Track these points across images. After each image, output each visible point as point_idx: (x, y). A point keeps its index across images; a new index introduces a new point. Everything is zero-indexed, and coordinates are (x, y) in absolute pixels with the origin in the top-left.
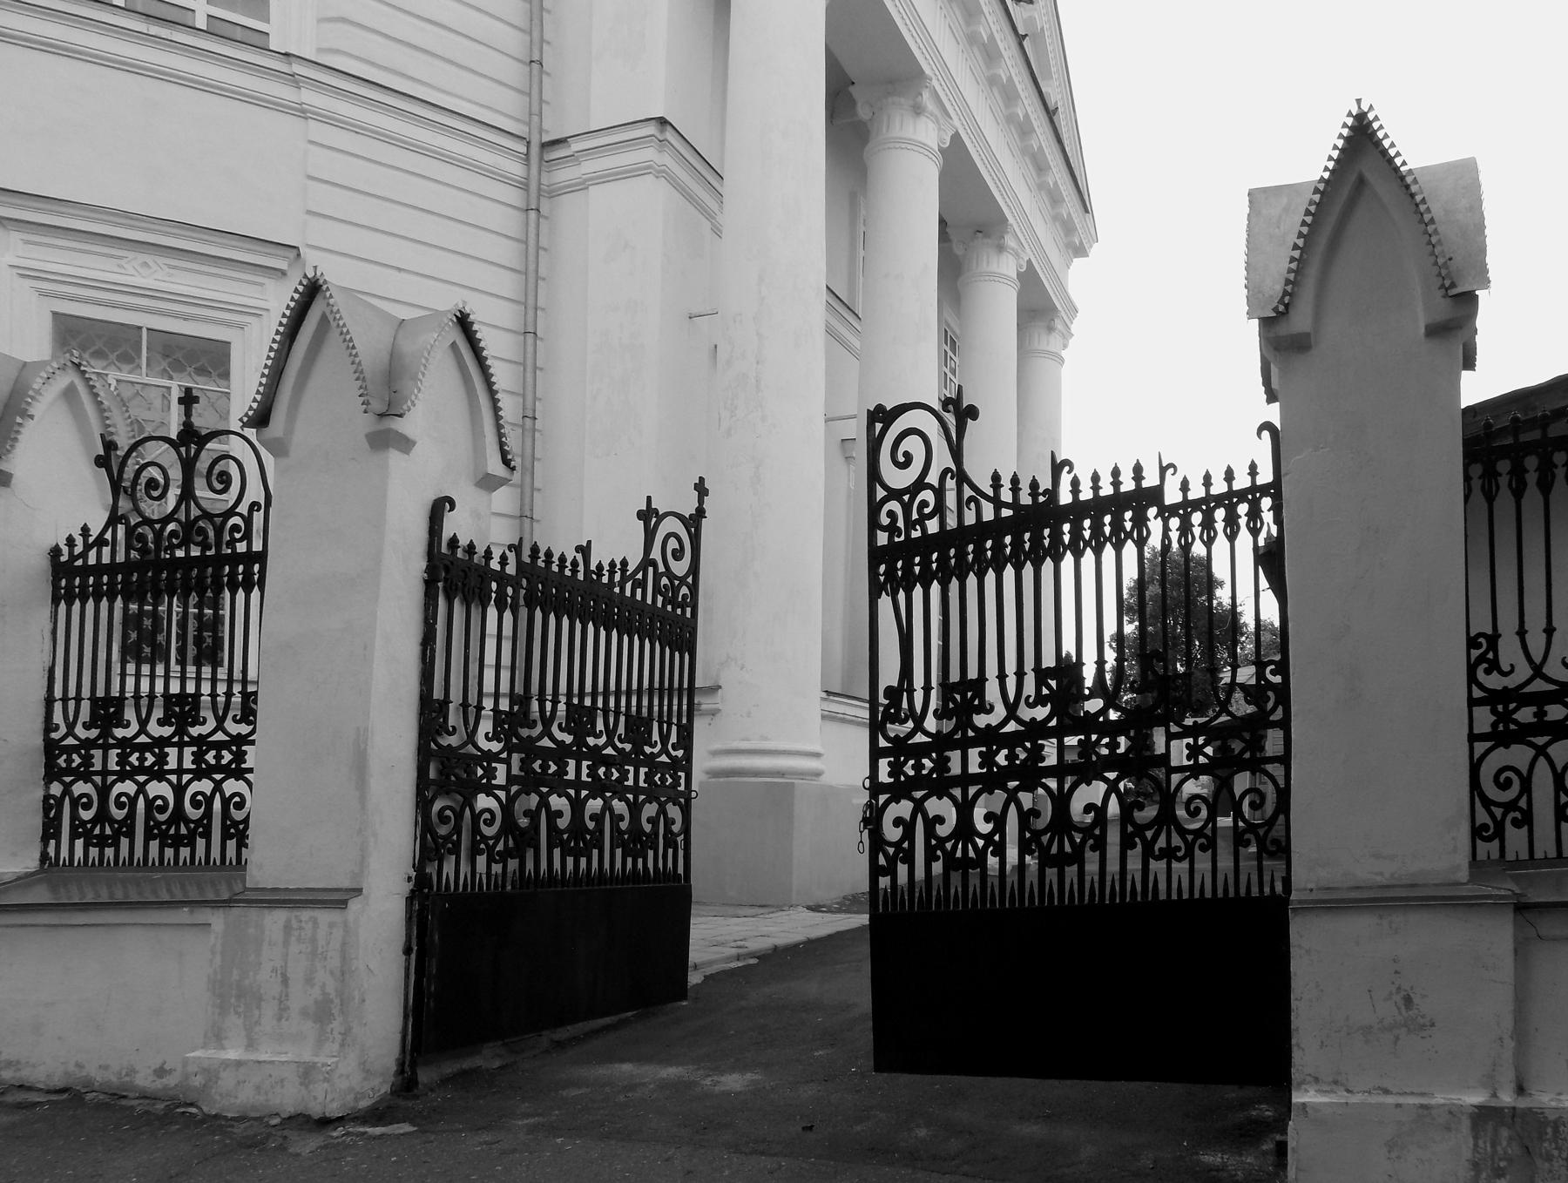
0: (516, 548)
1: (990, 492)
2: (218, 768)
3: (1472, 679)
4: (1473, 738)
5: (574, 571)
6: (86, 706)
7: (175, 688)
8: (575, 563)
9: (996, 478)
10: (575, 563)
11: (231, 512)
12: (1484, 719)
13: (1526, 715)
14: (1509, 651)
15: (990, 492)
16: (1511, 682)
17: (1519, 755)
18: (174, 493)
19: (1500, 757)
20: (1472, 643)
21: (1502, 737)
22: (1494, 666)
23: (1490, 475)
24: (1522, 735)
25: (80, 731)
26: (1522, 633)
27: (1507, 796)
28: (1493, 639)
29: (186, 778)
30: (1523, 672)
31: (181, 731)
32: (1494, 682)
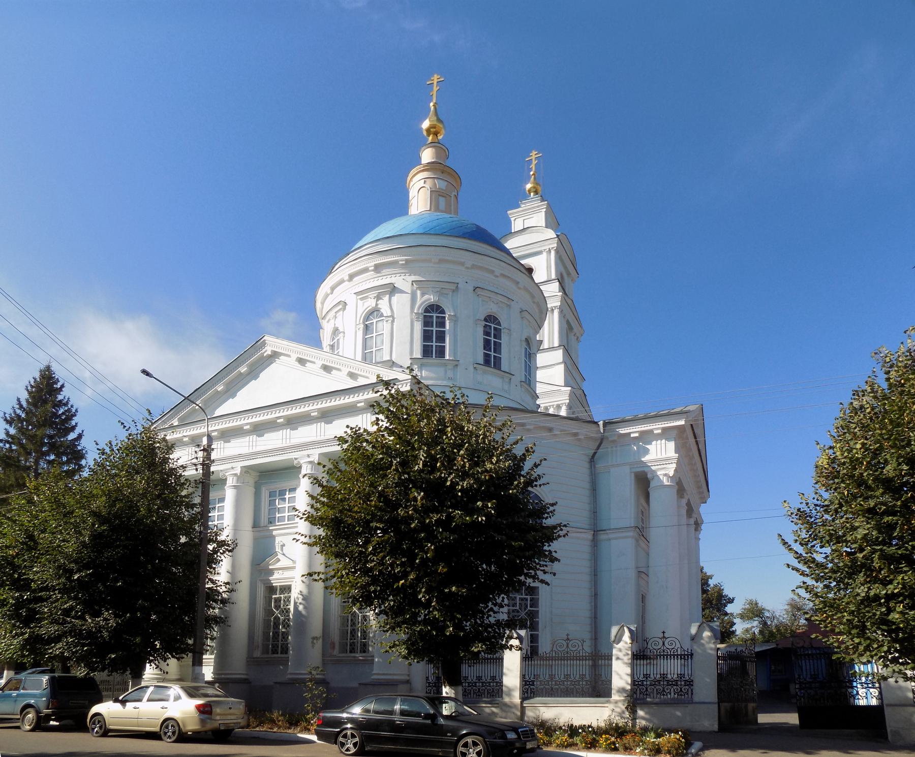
12: (427, 684)
14: (430, 678)
30: (653, 678)
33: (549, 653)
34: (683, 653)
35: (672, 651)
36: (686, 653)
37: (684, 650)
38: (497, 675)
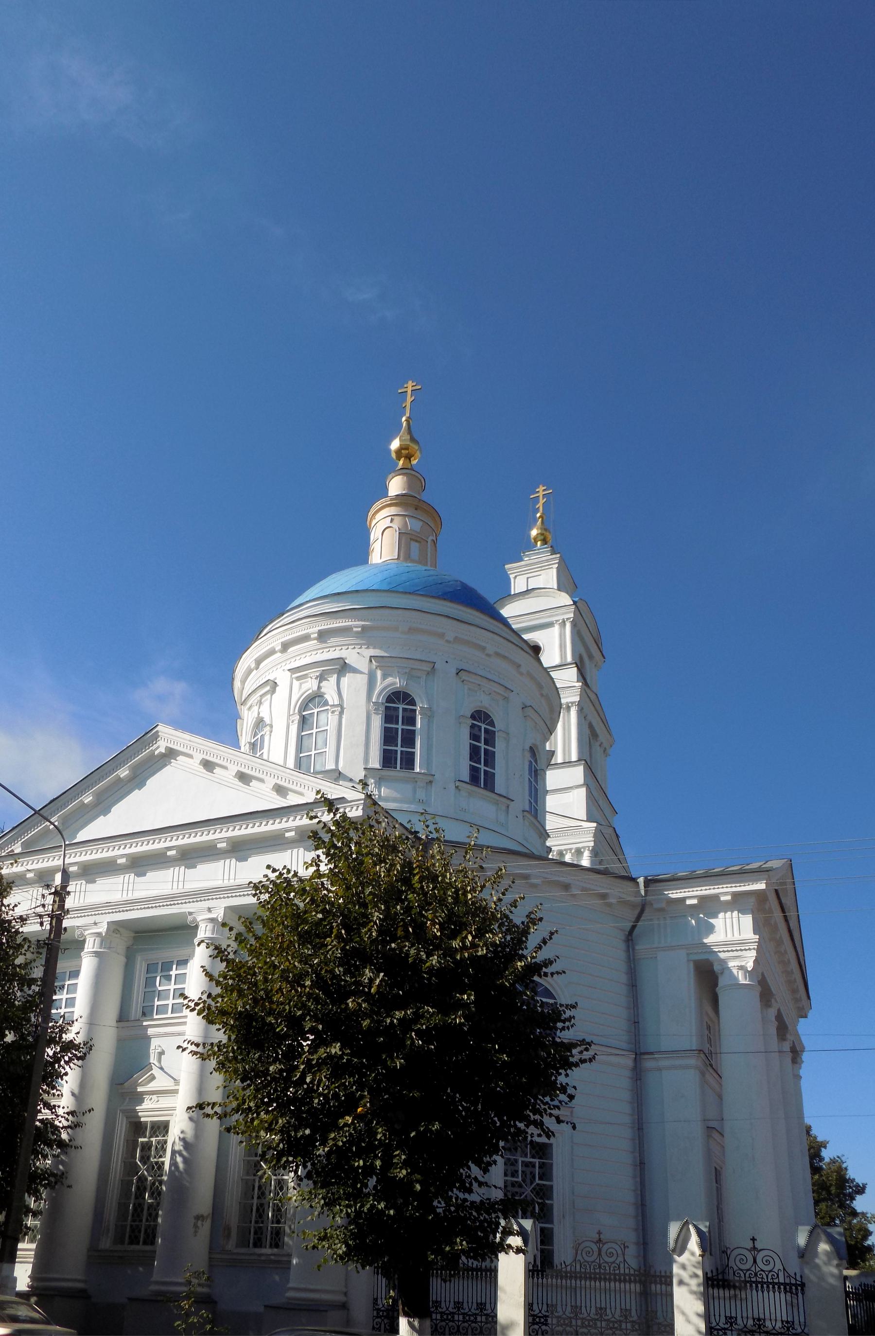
0: (860, 1285)
1: (794, 1276)
2: (540, 1323)
3: (374, 1307)
4: (374, 1316)
5: (859, 1290)
6: (452, 1303)
7: (479, 1301)
8: (858, 1288)
9: (795, 1274)
10: (858, 1288)
11: (614, 1262)
12: (375, 1313)
13: (537, 1320)
15: (794, 1276)
16: (443, 1310)
17: (379, 1320)
18: (596, 1254)
19: (377, 1320)
20: (374, 1299)
21: (533, 1324)
22: (532, 1310)
23: (533, 1275)
24: (537, 1323)
25: (450, 1309)
26: (445, 1301)
27: (378, 1327)
28: (377, 1298)
29: (438, 1322)
30: (445, 1309)
31: (481, 1311)
32: (377, 1307)
33: (571, 1265)
34: (787, 1281)
35: (770, 1277)
36: (793, 1281)
37: (789, 1276)
38: (465, 1301)
